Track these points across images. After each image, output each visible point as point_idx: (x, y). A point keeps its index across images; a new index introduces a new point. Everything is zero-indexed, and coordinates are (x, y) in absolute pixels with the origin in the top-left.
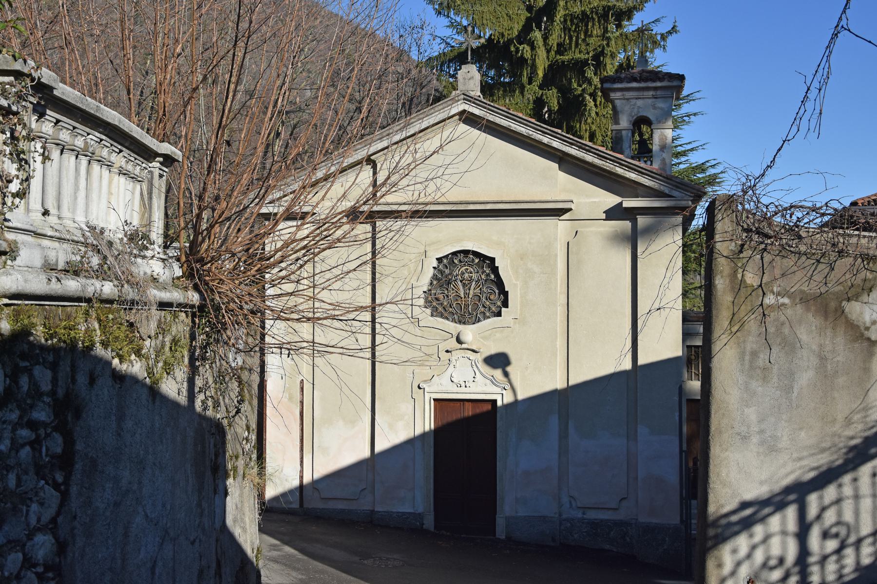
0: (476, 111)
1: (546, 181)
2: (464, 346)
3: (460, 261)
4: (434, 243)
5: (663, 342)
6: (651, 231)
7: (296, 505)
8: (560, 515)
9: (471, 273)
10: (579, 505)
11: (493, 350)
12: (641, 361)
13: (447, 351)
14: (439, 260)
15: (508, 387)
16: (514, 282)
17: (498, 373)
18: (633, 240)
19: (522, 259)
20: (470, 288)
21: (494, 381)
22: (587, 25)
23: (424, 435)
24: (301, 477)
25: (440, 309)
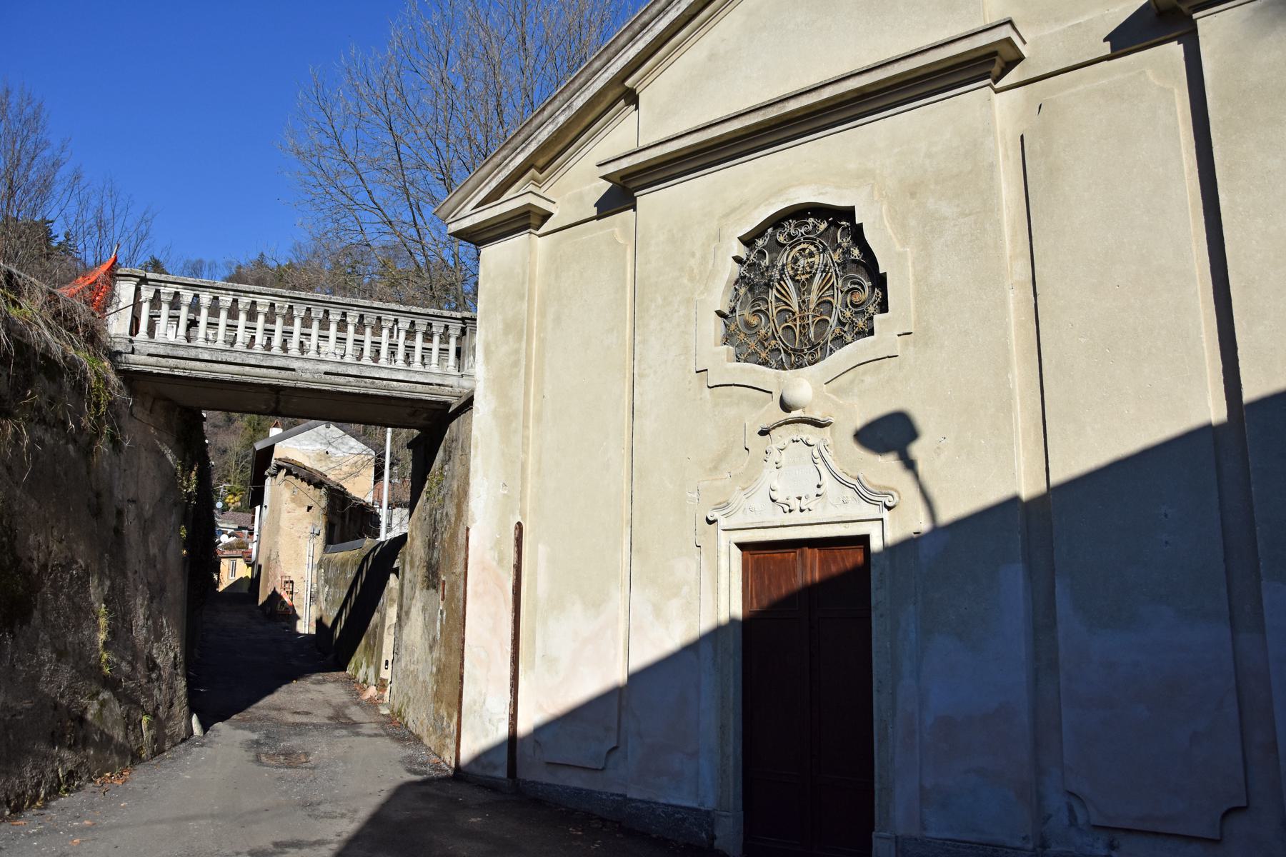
2: (795, 414)
4: (734, 210)
7: (502, 773)
8: (1044, 845)
9: (811, 255)
10: (1096, 820)
12: (1250, 393)
13: (764, 433)
16: (898, 248)
23: (718, 633)
24: (513, 717)
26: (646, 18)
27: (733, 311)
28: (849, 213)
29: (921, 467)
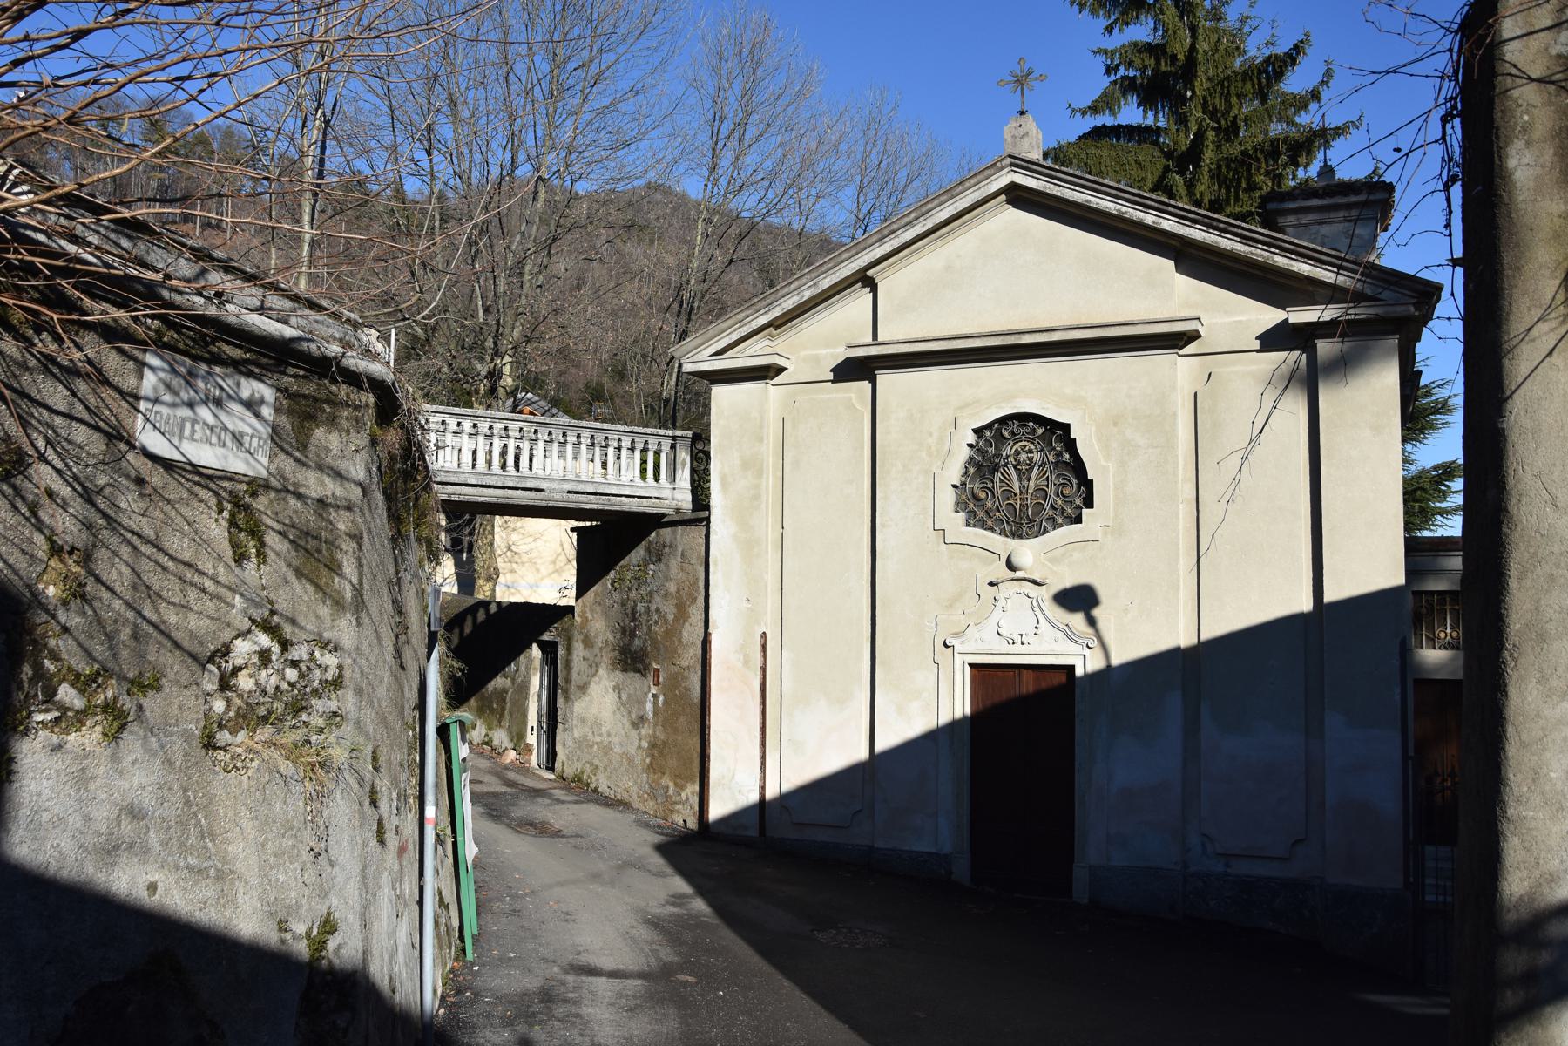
0: (1033, 183)
1: (1149, 288)
2: (1019, 574)
3: (1013, 434)
4: (968, 405)
5: (1370, 562)
6: (1343, 366)
7: (753, 832)
9: (1030, 451)
11: (1068, 582)
12: (1330, 596)
13: (991, 584)
14: (978, 432)
15: (1094, 643)
17: (1077, 620)
18: (1309, 382)
19: (1115, 424)
20: (1028, 477)
21: (1070, 635)
22: (1249, 170)
23: (954, 726)
24: (763, 788)
25: (981, 514)
26: (895, 226)
27: (963, 484)
28: (1066, 428)
29: (1101, 625)
